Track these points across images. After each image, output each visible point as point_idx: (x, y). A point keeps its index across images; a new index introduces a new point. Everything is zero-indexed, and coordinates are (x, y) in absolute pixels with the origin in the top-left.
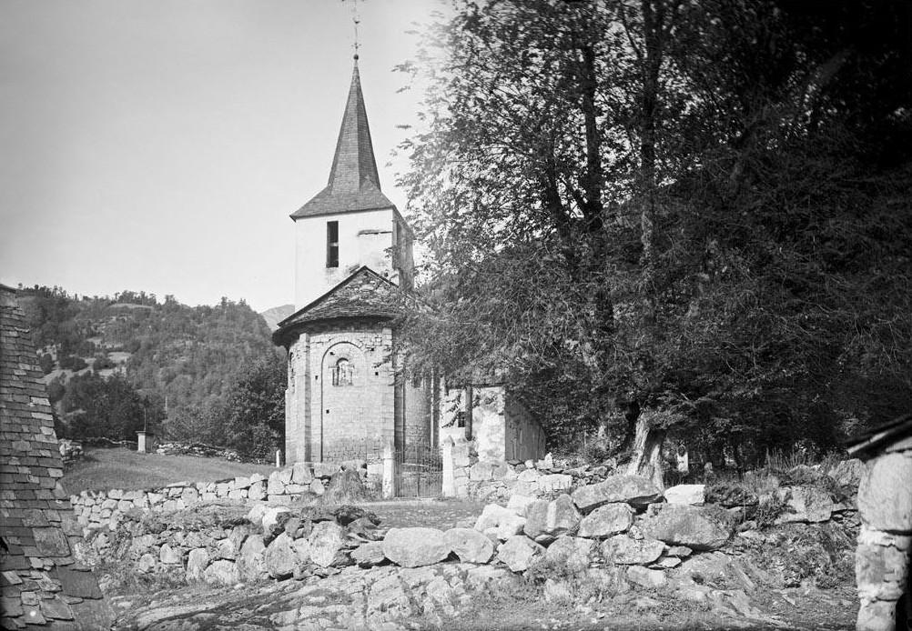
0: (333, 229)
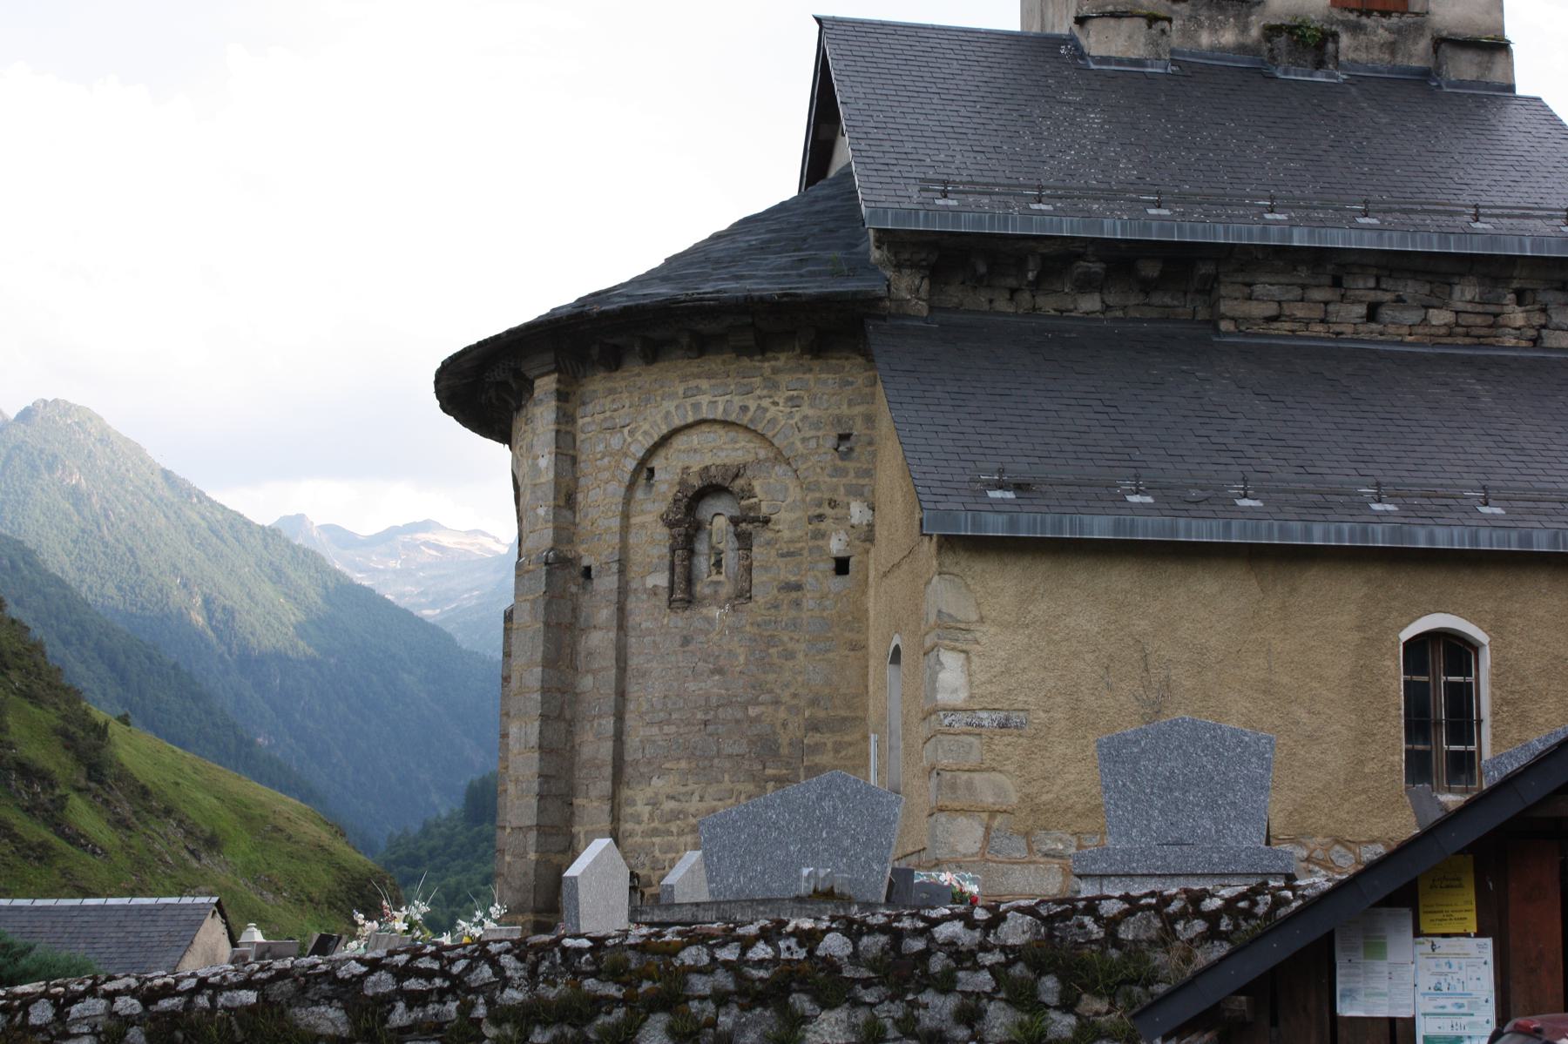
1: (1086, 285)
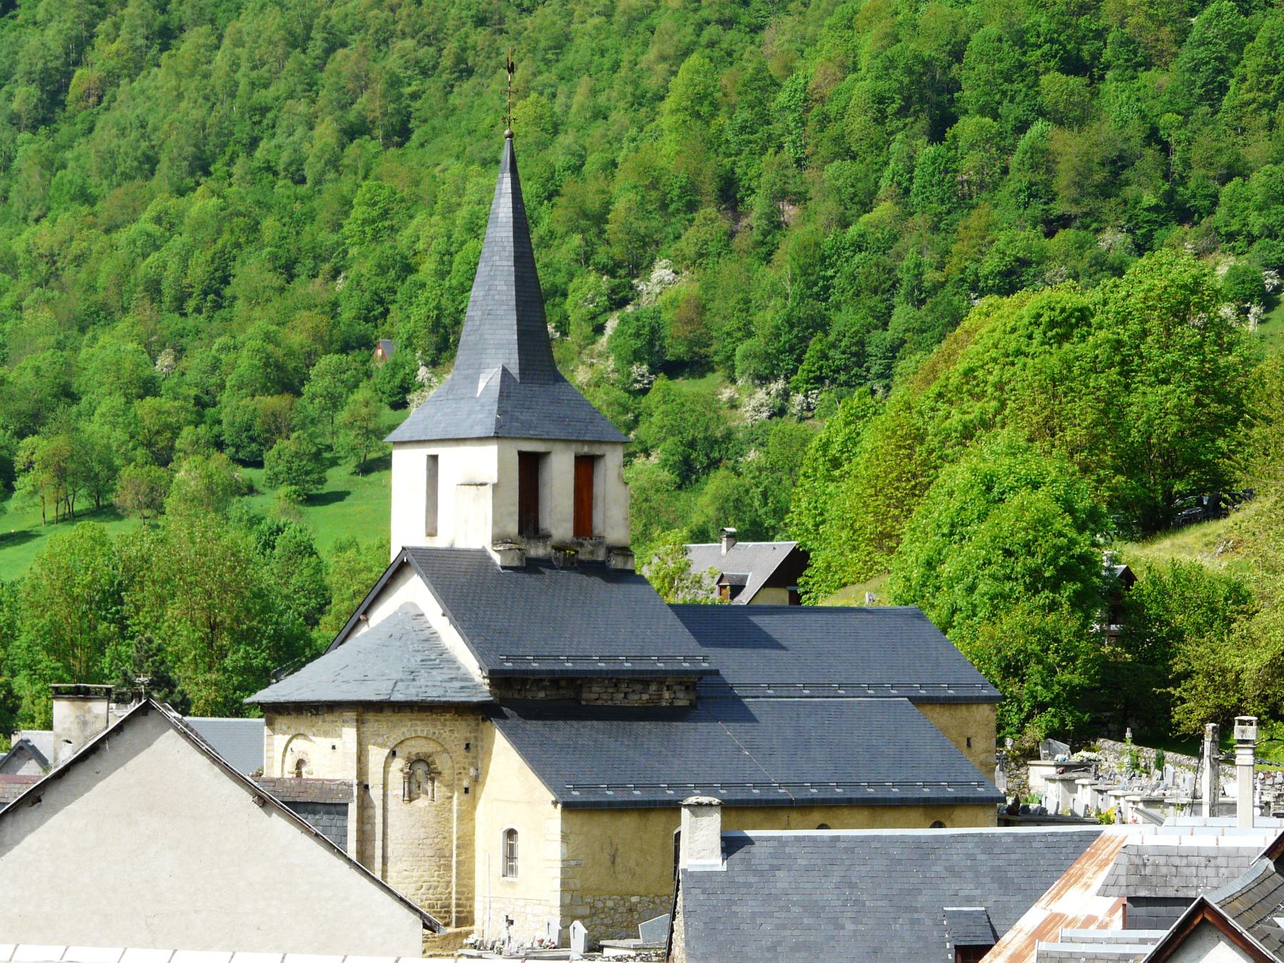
1: (544, 688)
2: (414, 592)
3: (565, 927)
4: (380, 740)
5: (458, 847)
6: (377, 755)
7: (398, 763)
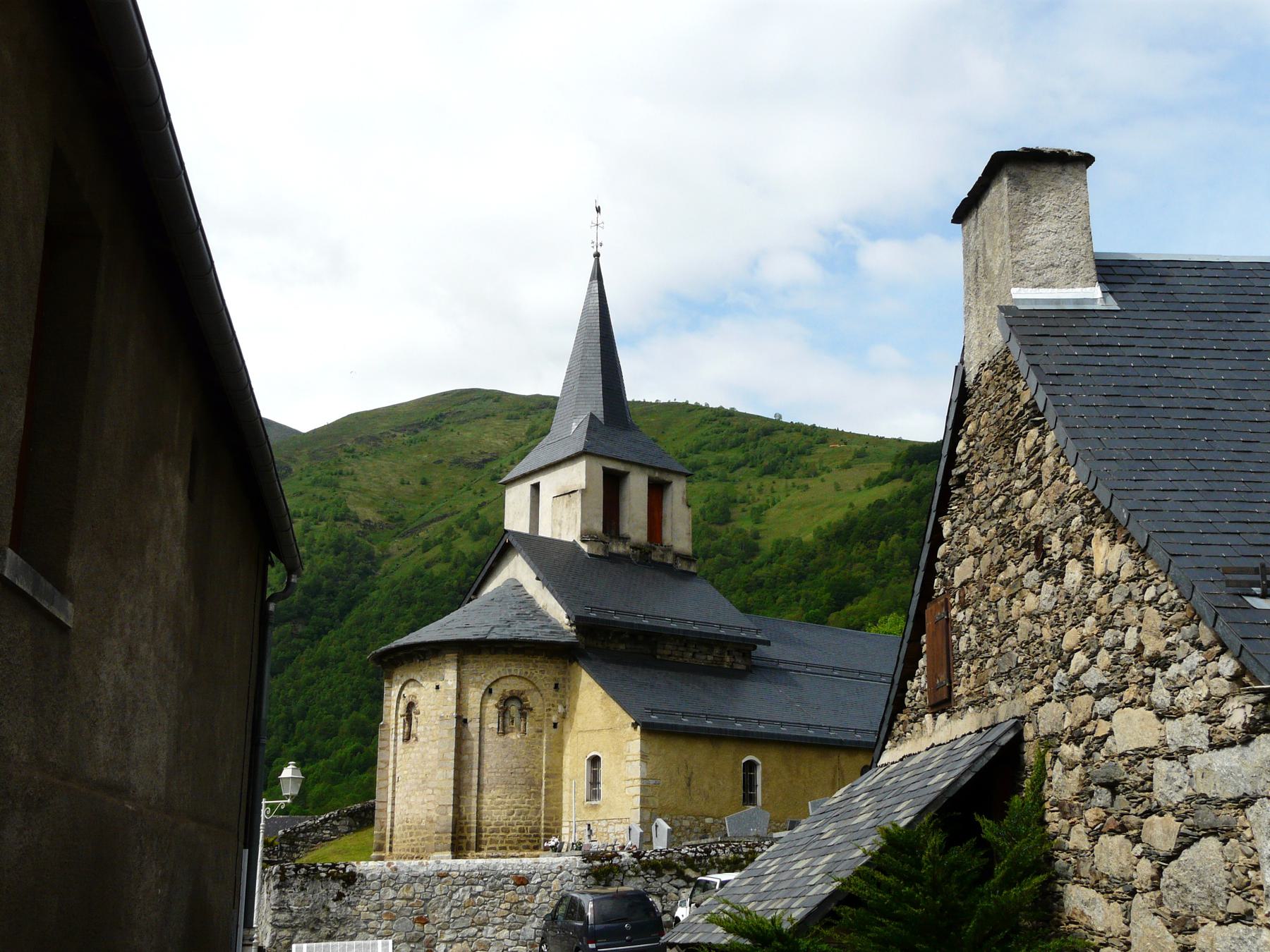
0: (536, 487)
2: (518, 570)
3: (646, 824)
4: (478, 678)
5: (547, 776)
6: (474, 696)
7: (492, 703)
